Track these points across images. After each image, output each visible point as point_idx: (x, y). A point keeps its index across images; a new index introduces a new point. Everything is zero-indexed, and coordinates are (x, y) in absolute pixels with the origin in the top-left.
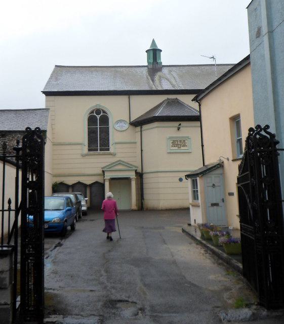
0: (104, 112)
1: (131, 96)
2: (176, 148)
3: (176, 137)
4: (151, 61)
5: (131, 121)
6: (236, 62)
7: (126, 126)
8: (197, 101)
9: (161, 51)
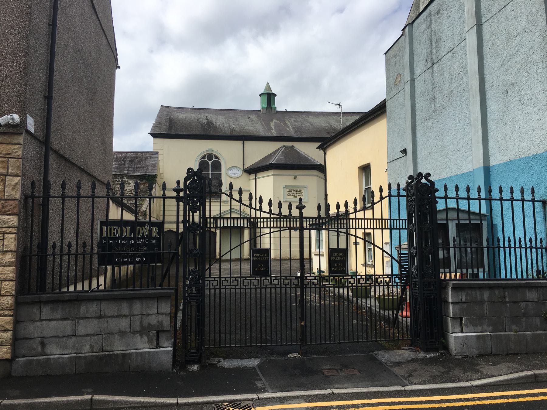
0: (216, 157)
1: (245, 142)
2: (292, 197)
3: (292, 186)
4: (265, 105)
5: (245, 168)
6: (366, 111)
7: (240, 172)
8: (322, 149)
9: (275, 95)
